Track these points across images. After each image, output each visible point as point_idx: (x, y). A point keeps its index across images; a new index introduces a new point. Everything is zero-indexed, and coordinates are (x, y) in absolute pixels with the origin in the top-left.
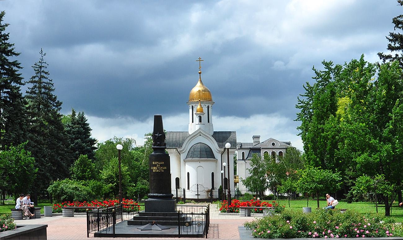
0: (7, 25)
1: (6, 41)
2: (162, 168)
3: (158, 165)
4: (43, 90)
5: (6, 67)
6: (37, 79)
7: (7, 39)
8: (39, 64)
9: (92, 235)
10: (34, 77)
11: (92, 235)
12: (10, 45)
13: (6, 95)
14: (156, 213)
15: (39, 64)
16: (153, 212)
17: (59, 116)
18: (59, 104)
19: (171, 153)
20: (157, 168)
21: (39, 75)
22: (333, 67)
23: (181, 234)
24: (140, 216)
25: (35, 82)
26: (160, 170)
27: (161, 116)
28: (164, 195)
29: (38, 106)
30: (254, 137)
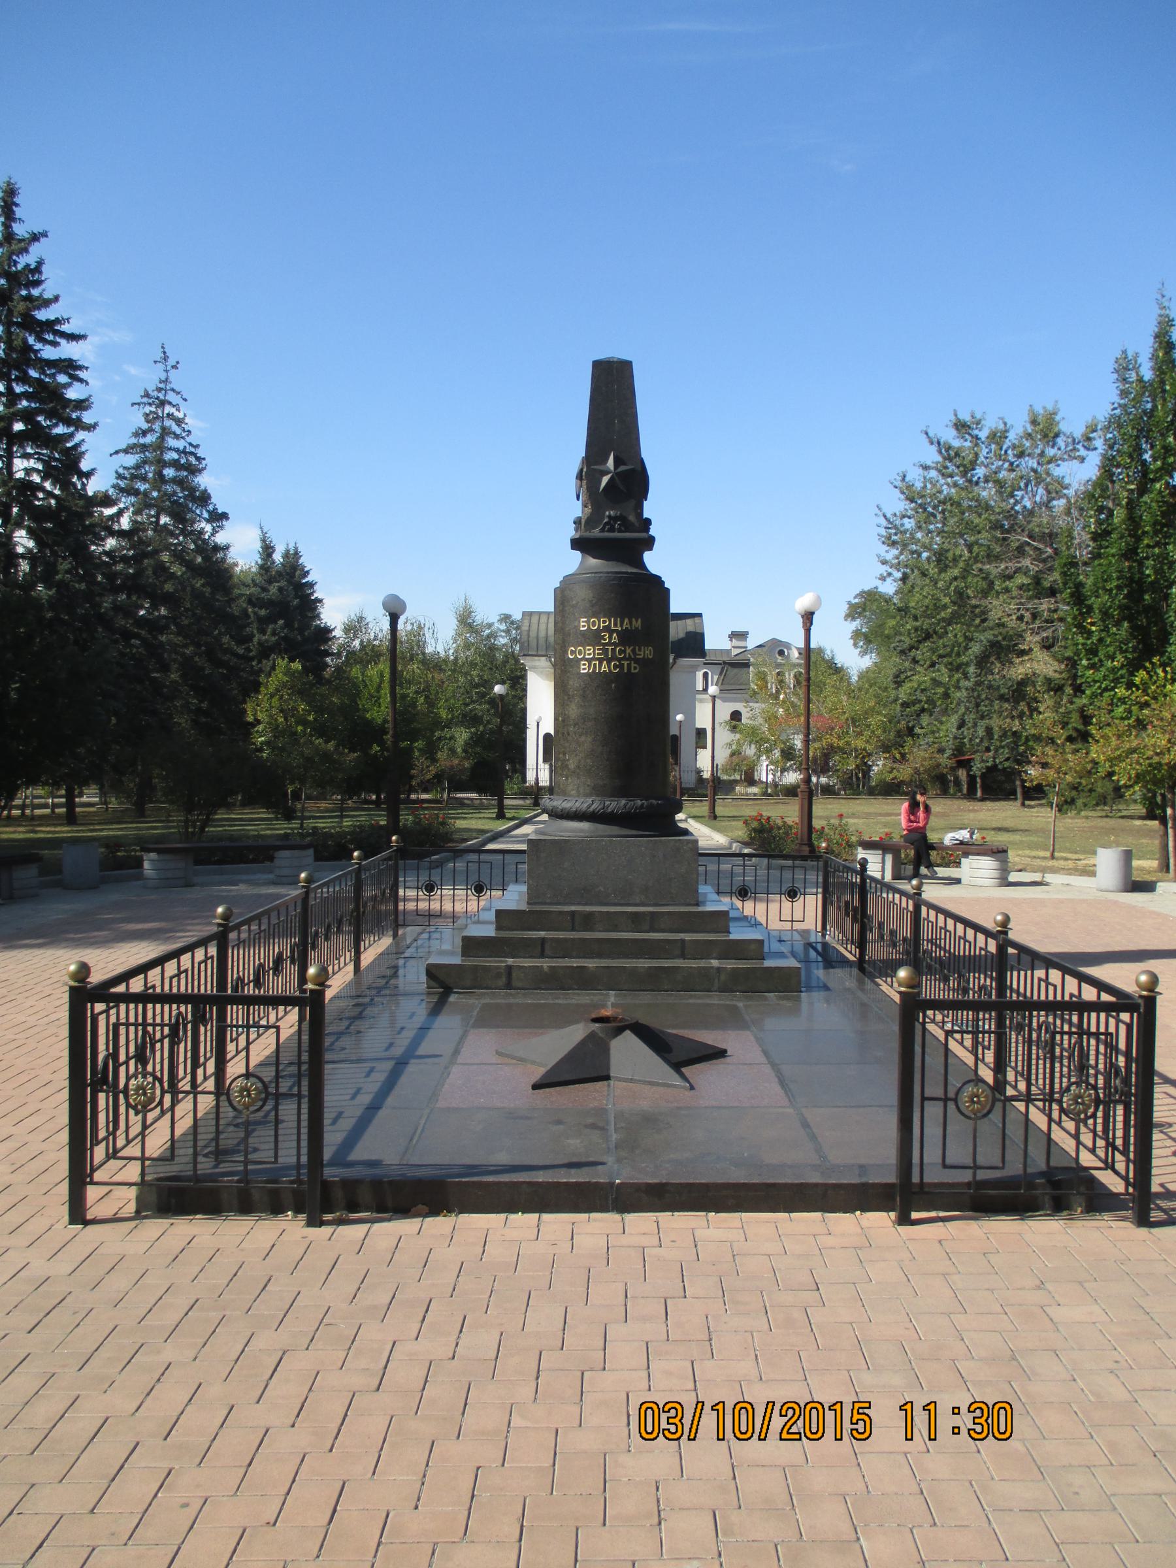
0: (35, 238)
1: (35, 292)
2: (628, 651)
3: (611, 632)
4: (169, 472)
5: (33, 374)
6: (149, 439)
7: (38, 283)
8: (155, 394)
9: (116, 1186)
10: (145, 433)
11: (116, 1186)
12: (47, 303)
13: (32, 463)
14: (591, 914)
15: (155, 394)
16: (591, 904)
17: (217, 548)
18: (218, 518)
19: (533, 668)
20: (605, 652)
21: (157, 426)
22: (983, 435)
23: (916, 1179)
24: (498, 928)
25: (144, 448)
26: (621, 666)
27: (628, 364)
28: (639, 803)
29: (153, 519)
30: (734, 635)
